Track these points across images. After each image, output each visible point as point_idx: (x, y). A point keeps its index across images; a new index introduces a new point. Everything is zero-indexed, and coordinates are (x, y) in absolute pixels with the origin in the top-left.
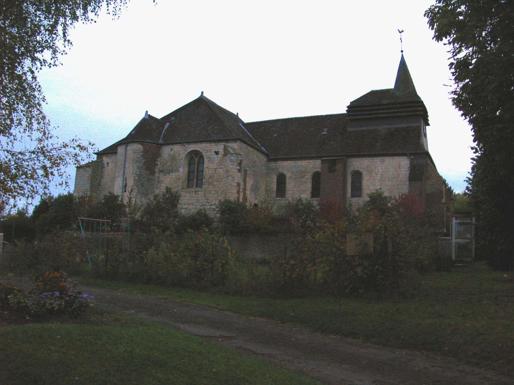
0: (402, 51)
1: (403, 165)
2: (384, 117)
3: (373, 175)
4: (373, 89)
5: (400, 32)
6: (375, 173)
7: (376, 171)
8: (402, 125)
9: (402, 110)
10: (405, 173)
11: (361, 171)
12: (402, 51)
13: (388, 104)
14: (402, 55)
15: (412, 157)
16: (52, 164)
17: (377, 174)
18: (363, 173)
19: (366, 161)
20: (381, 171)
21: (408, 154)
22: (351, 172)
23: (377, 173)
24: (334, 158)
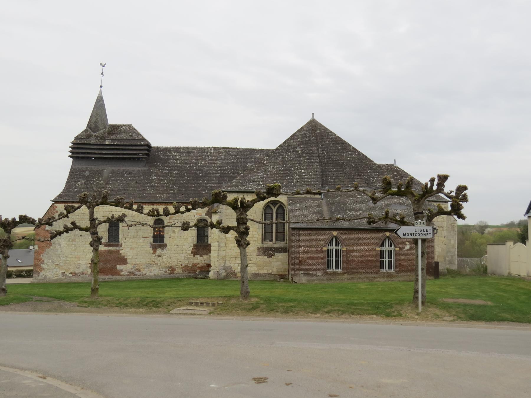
0: (101, 87)
12: (101, 87)
14: (101, 91)
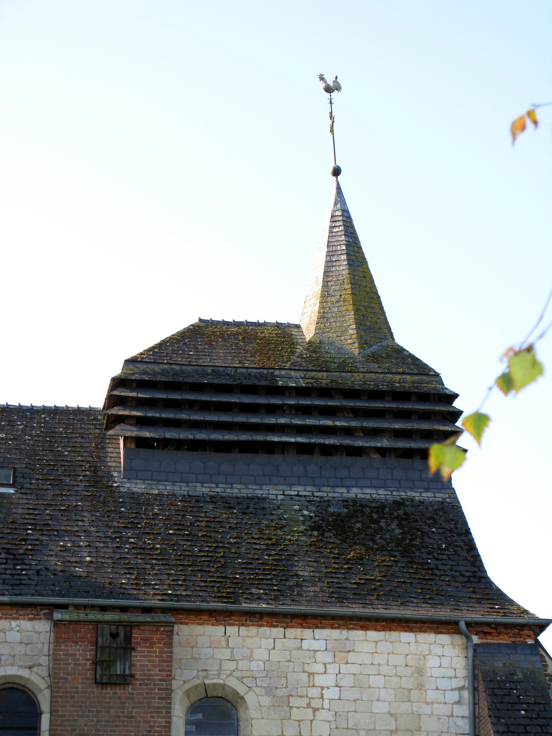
0: (337, 172)
1: (436, 672)
2: (284, 447)
3: (296, 714)
4: (206, 317)
5: (328, 90)
6: (309, 706)
7: (313, 692)
8: (354, 490)
9: (255, 420)
10: (445, 710)
11: (241, 689)
13: (301, 392)
15: (476, 639)
16: (305, 519)
17: (315, 710)
18: (250, 698)
19: (264, 642)
20: (331, 694)
21: (463, 625)
22: (187, 693)
23: (316, 704)
24: (125, 617)
